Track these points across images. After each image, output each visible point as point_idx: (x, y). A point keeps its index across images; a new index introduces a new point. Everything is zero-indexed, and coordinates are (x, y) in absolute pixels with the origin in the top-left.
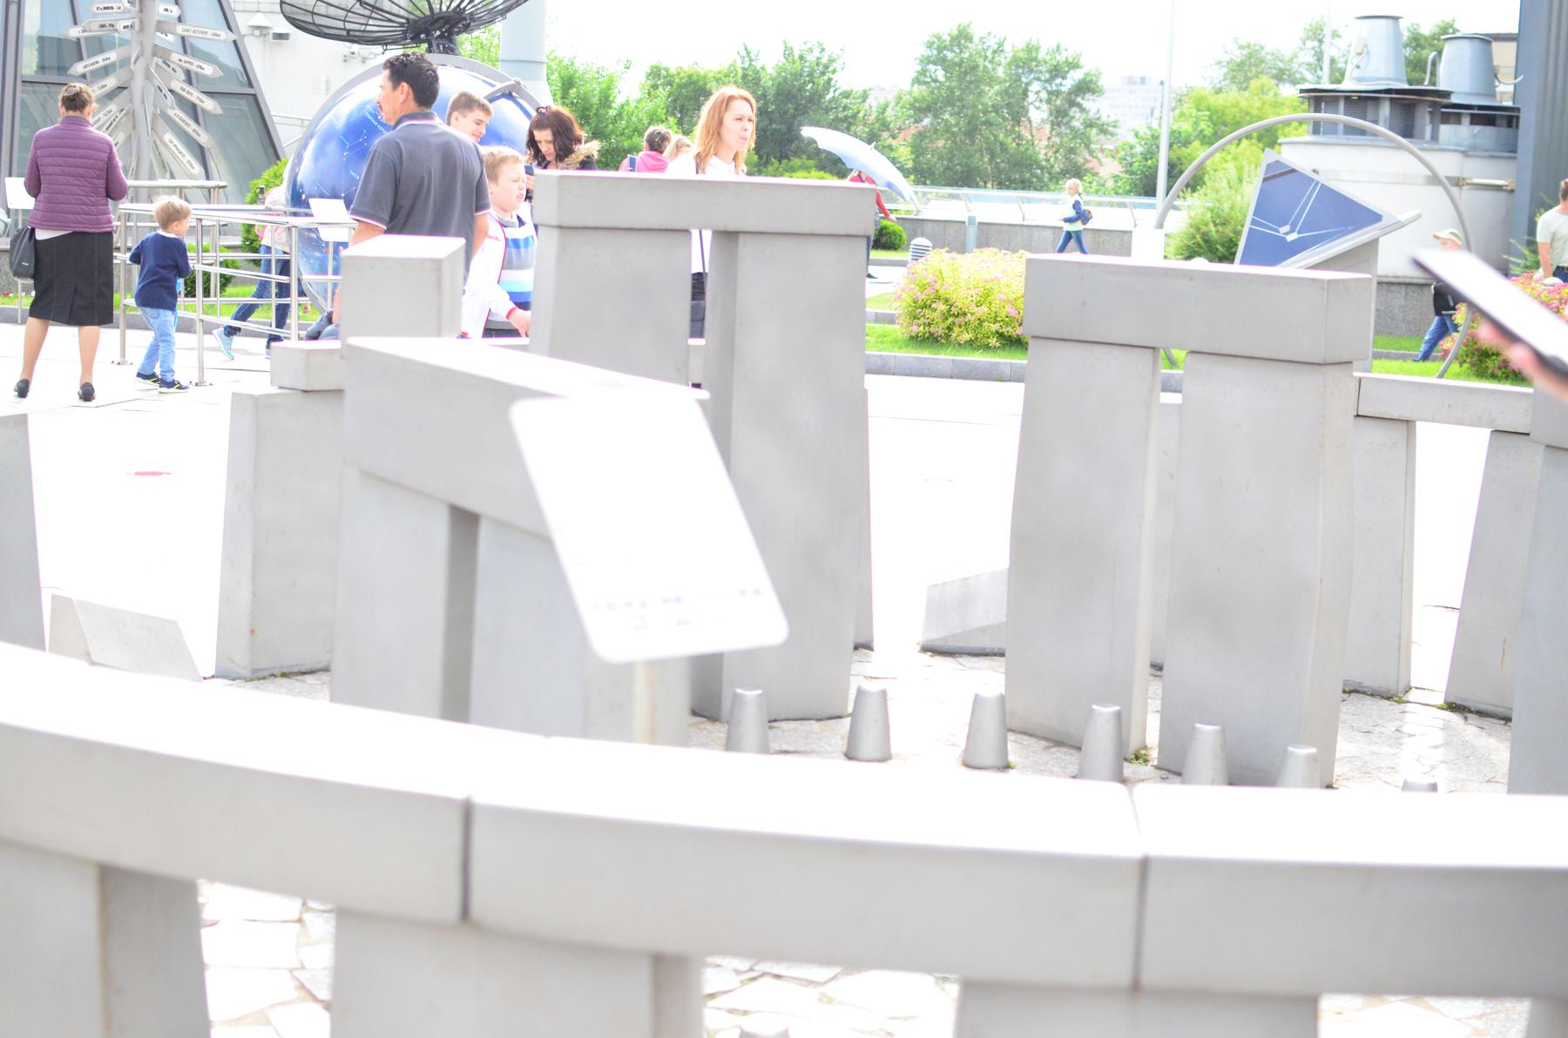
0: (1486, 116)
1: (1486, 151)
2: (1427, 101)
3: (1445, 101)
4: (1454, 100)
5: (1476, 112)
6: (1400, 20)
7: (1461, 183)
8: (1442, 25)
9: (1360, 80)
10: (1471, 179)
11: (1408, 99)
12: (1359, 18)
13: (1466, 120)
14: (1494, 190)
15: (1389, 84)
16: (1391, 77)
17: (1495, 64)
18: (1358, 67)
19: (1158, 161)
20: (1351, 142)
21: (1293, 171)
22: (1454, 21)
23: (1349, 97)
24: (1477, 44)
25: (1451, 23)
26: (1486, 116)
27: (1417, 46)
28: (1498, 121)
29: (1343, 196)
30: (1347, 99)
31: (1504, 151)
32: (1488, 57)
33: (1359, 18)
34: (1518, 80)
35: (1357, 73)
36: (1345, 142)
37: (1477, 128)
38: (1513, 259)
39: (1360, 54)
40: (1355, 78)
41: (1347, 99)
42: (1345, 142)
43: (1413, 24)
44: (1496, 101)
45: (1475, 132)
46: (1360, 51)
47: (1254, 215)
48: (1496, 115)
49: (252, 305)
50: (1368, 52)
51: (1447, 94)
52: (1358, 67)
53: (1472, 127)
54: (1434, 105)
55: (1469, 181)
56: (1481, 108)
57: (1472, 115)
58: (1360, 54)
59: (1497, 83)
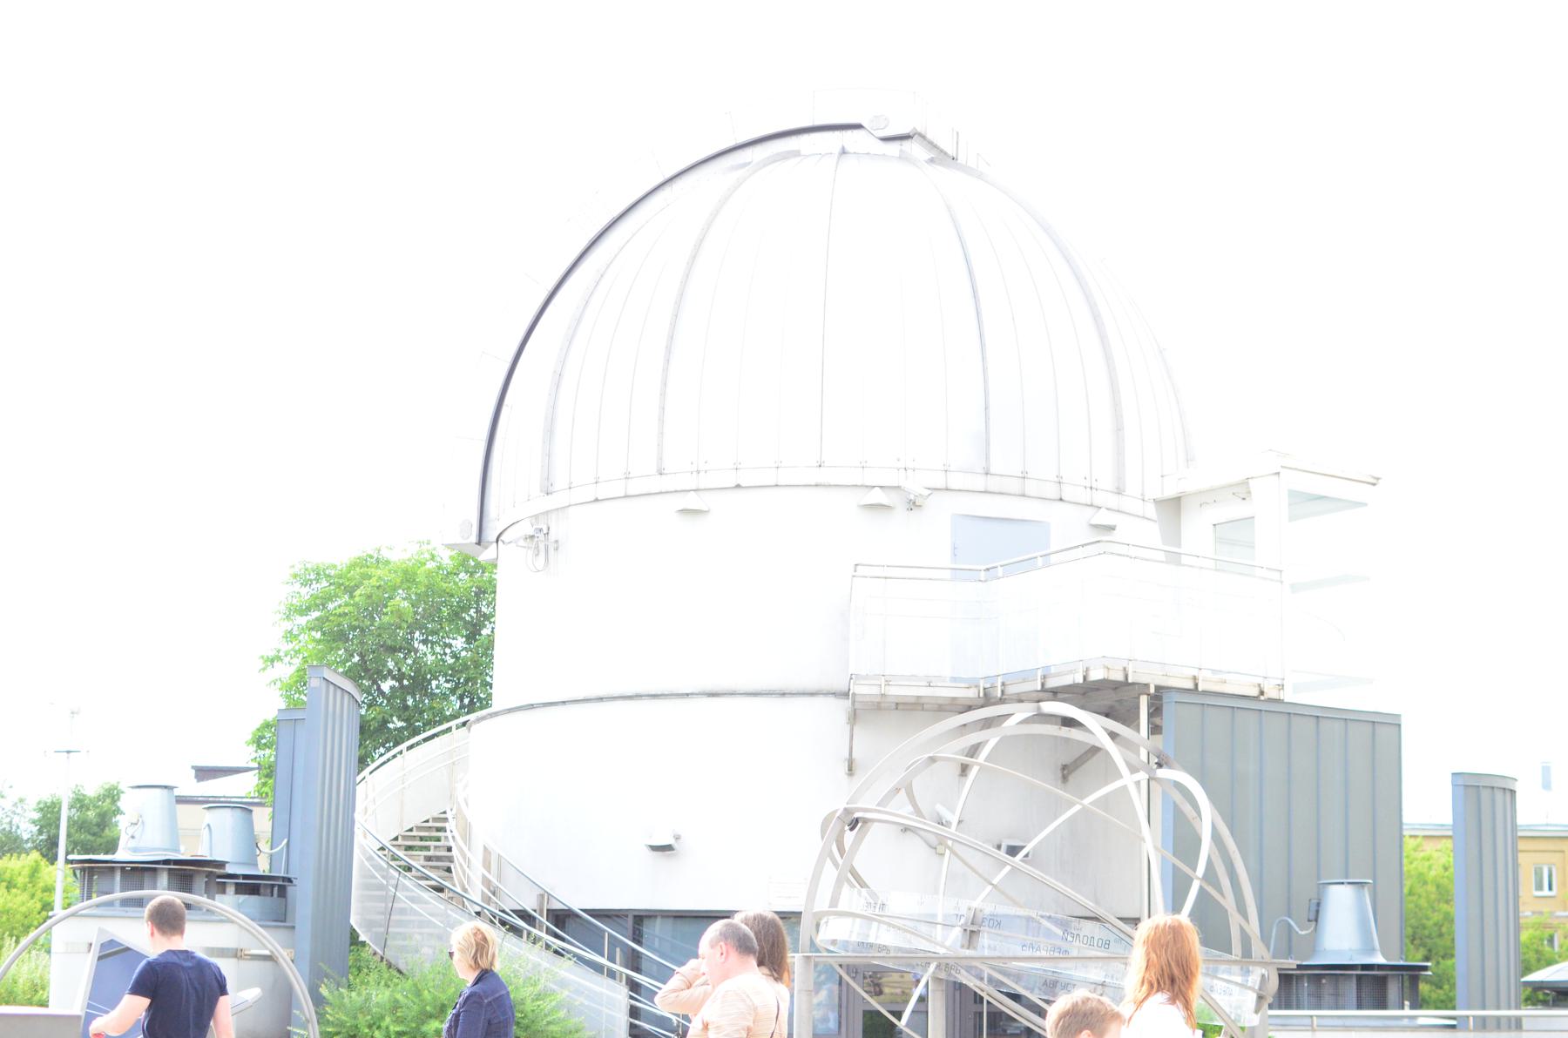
0: (250, 886)
1: (582, 924)
2: (204, 871)
3: (221, 871)
4: (229, 870)
5: (241, 881)
6: (175, 790)
7: (239, 954)
8: (107, 787)
9: (135, 850)
10: (250, 950)
11: (185, 870)
12: (133, 787)
13: (231, 890)
14: (259, 960)
15: (165, 855)
16: (166, 847)
17: (256, 833)
18: (133, 837)
19: (1453, 940)
20: (129, 914)
21: (128, 949)
22: (118, 783)
23: (124, 867)
24: (238, 813)
25: (116, 785)
26: (250, 886)
27: (81, 807)
28: (262, 890)
30: (123, 869)
31: (269, 920)
32: (250, 825)
33: (133, 787)
34: (274, 851)
35: (132, 844)
36: (124, 914)
37: (242, 898)
38: (295, 1030)
39: (136, 824)
40: (129, 849)
41: (123, 869)
42: (124, 914)
43: (77, 786)
44: (258, 870)
45: (240, 901)
46: (135, 821)
47: (89, 999)
48: (260, 884)
50: (143, 822)
51: (221, 864)
52: (133, 837)
53: (237, 896)
54: (209, 875)
55: (246, 952)
56: (246, 877)
57: (237, 884)
58: (136, 824)
59: (258, 852)
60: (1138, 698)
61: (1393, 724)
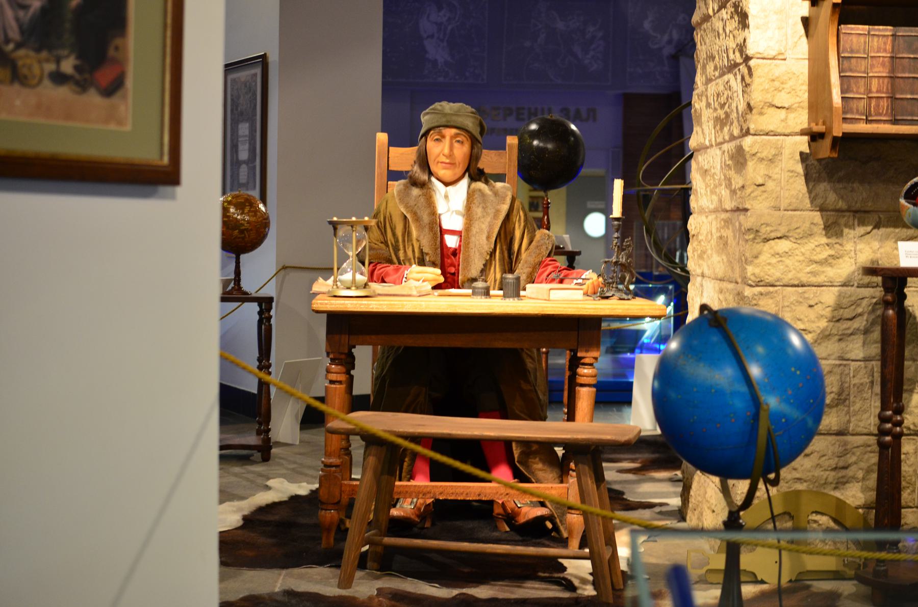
29: (280, 24)
49: (363, 579)
60: (352, 234)
61: (221, 532)
